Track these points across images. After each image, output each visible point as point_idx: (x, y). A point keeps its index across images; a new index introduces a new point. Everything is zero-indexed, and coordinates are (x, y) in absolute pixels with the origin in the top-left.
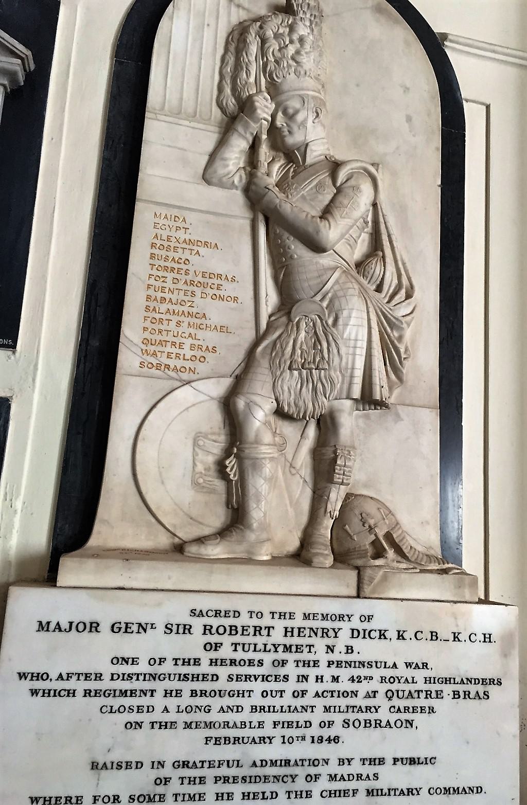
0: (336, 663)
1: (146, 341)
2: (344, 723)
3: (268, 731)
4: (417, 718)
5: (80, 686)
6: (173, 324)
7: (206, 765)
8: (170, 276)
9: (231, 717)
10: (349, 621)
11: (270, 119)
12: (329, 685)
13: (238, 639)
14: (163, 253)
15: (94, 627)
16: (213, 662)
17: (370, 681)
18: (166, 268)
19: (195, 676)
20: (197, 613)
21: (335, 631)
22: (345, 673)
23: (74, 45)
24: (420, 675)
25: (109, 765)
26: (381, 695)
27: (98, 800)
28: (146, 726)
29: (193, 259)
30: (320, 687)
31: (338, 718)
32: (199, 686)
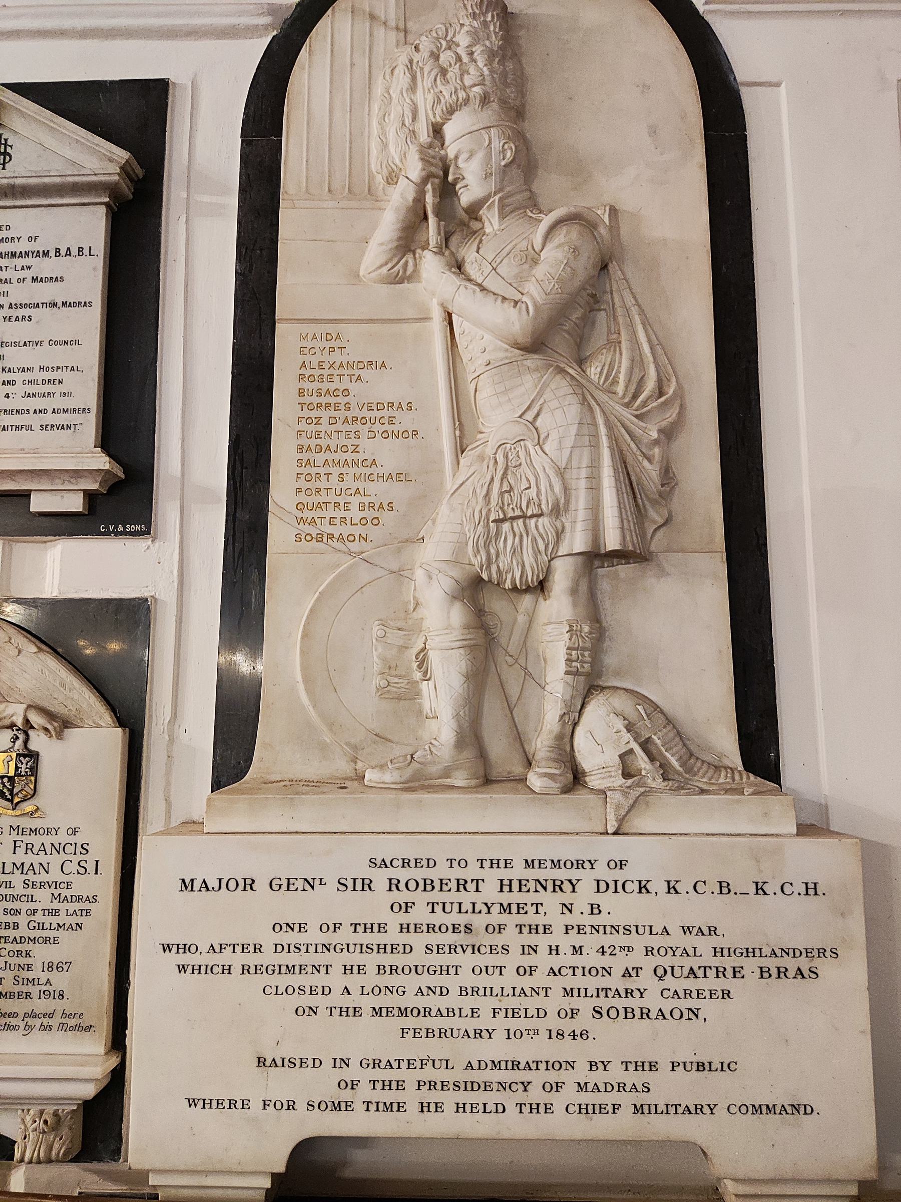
0: (576, 928)
1: (300, 506)
2: (594, 1013)
3: (485, 1021)
4: (706, 1007)
5: (237, 960)
6: (334, 478)
7: (404, 1065)
8: (325, 415)
9: (434, 1002)
10: (592, 868)
11: (441, 173)
12: (567, 959)
13: (436, 896)
14: (315, 385)
15: (249, 884)
16: (404, 928)
17: (628, 953)
18: (319, 405)
19: (381, 946)
20: (378, 862)
21: (572, 883)
22: (590, 942)
23: (717, 5)
24: (705, 945)
25: (279, 1063)
26: (647, 973)
27: (269, 1105)
28: (323, 1012)
29: (353, 387)
30: (556, 962)
31: (585, 1005)
32: (387, 960)
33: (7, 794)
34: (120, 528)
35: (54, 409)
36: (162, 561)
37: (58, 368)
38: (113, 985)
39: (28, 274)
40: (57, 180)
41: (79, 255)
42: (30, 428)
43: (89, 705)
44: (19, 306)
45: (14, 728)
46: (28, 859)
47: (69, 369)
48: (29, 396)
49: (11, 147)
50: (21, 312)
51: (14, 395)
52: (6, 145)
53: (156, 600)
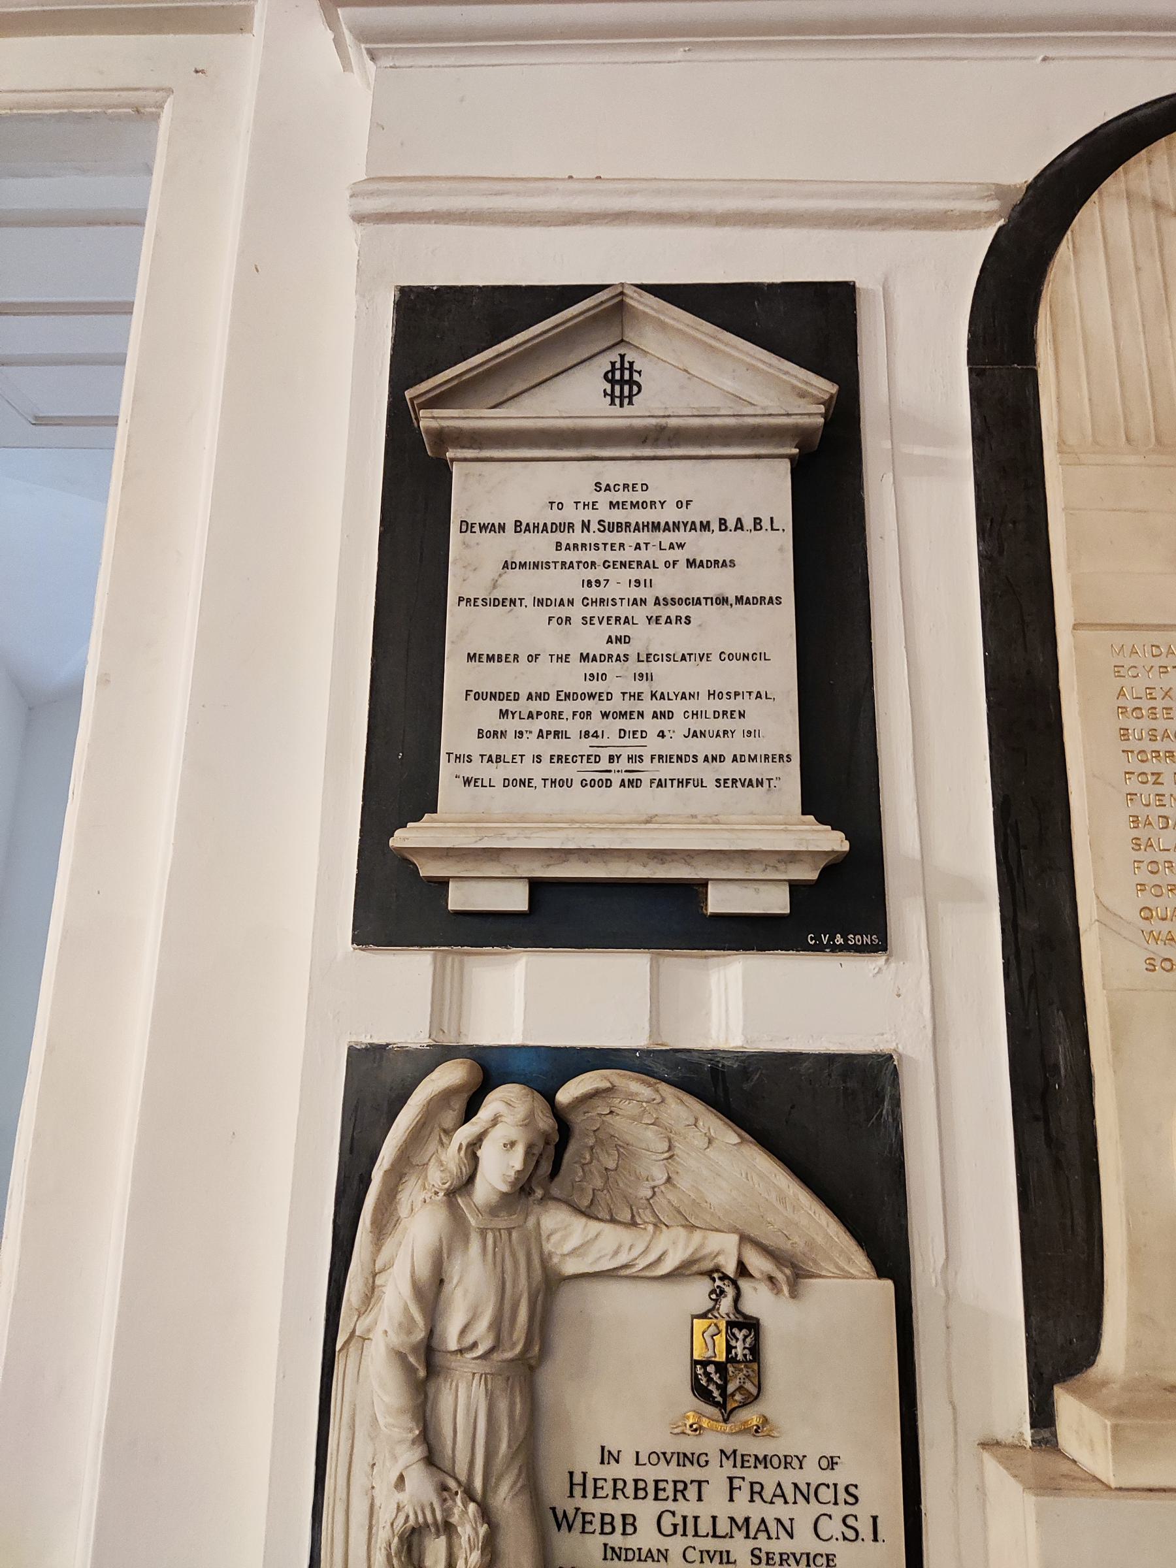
33: (716, 1393)
34: (839, 940)
35: (735, 756)
36: (903, 991)
37: (736, 694)
39: (680, 555)
40: (732, 421)
41: (755, 529)
42: (700, 783)
43: (827, 1236)
44: (670, 601)
45: (716, 1275)
46: (757, 1511)
47: (754, 695)
48: (695, 735)
49: (639, 373)
50: (674, 611)
51: (671, 734)
52: (631, 369)
53: (900, 1056)
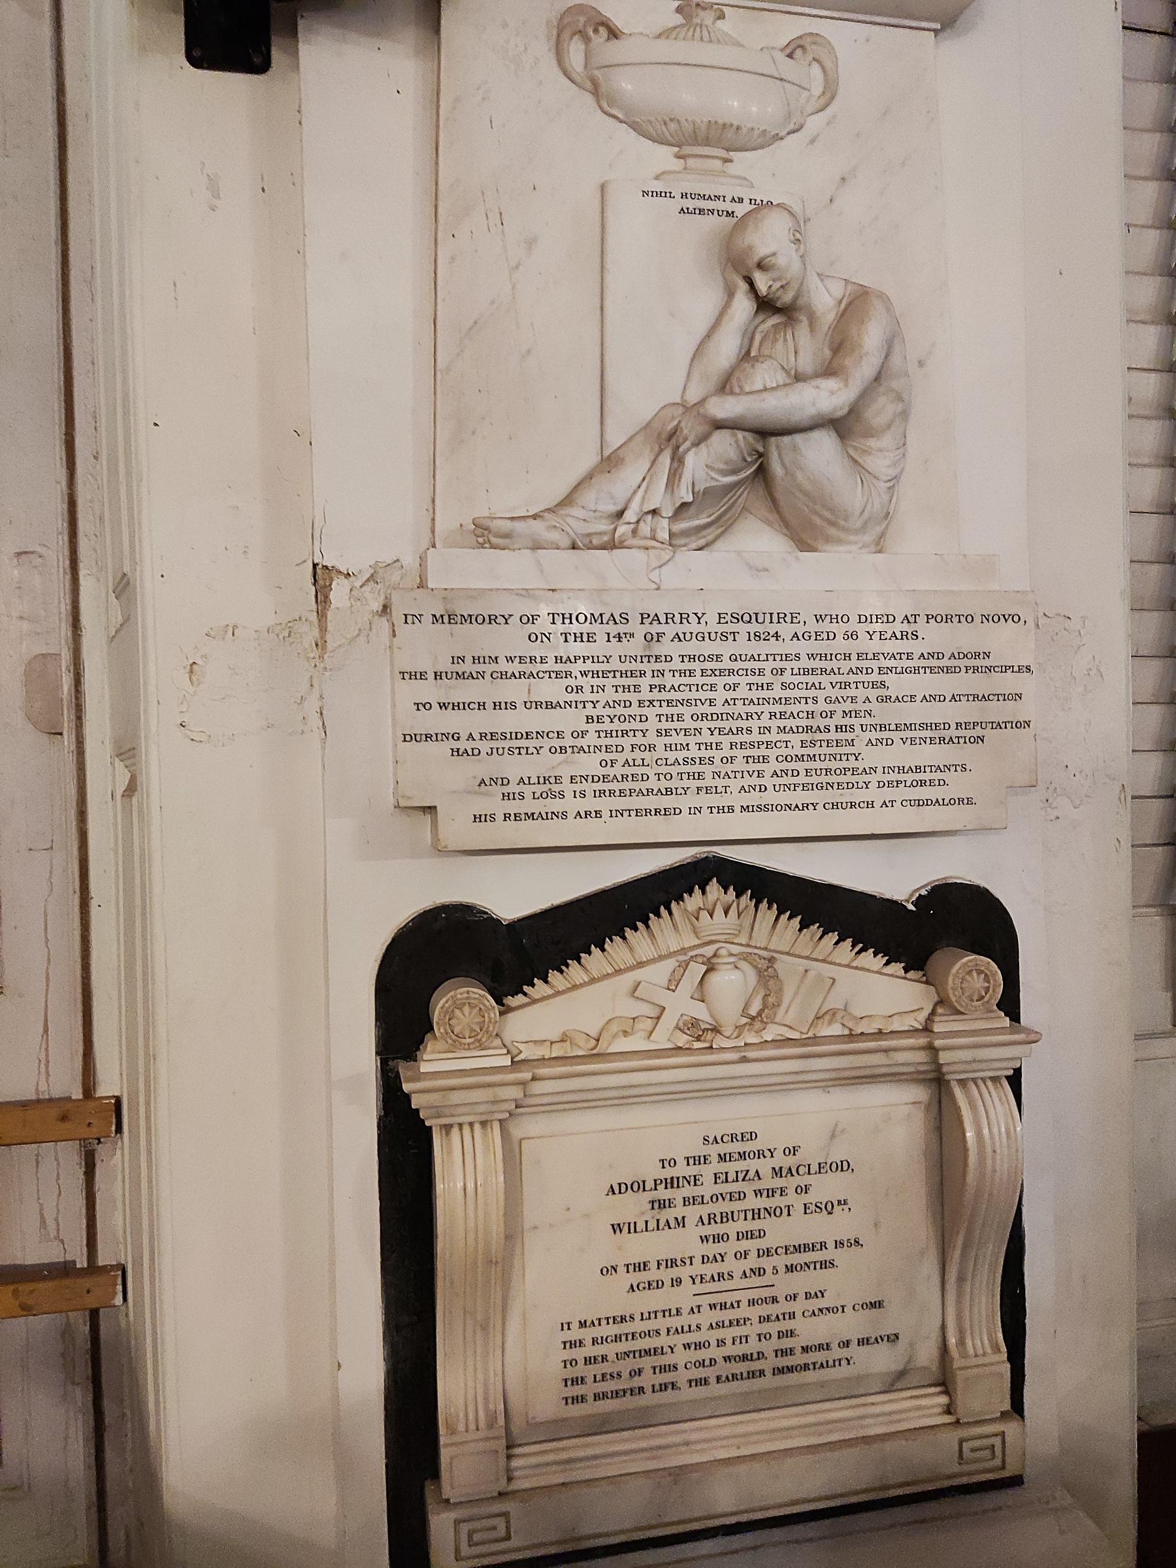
38: (380, 1103)
